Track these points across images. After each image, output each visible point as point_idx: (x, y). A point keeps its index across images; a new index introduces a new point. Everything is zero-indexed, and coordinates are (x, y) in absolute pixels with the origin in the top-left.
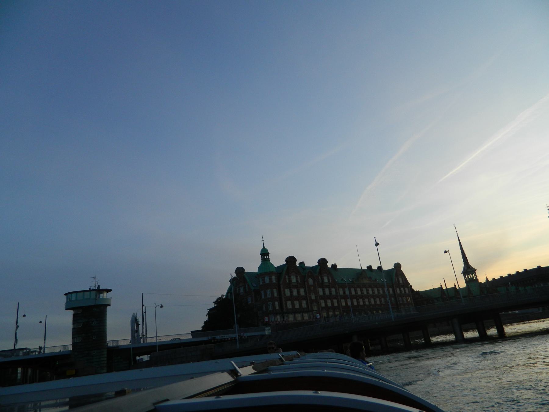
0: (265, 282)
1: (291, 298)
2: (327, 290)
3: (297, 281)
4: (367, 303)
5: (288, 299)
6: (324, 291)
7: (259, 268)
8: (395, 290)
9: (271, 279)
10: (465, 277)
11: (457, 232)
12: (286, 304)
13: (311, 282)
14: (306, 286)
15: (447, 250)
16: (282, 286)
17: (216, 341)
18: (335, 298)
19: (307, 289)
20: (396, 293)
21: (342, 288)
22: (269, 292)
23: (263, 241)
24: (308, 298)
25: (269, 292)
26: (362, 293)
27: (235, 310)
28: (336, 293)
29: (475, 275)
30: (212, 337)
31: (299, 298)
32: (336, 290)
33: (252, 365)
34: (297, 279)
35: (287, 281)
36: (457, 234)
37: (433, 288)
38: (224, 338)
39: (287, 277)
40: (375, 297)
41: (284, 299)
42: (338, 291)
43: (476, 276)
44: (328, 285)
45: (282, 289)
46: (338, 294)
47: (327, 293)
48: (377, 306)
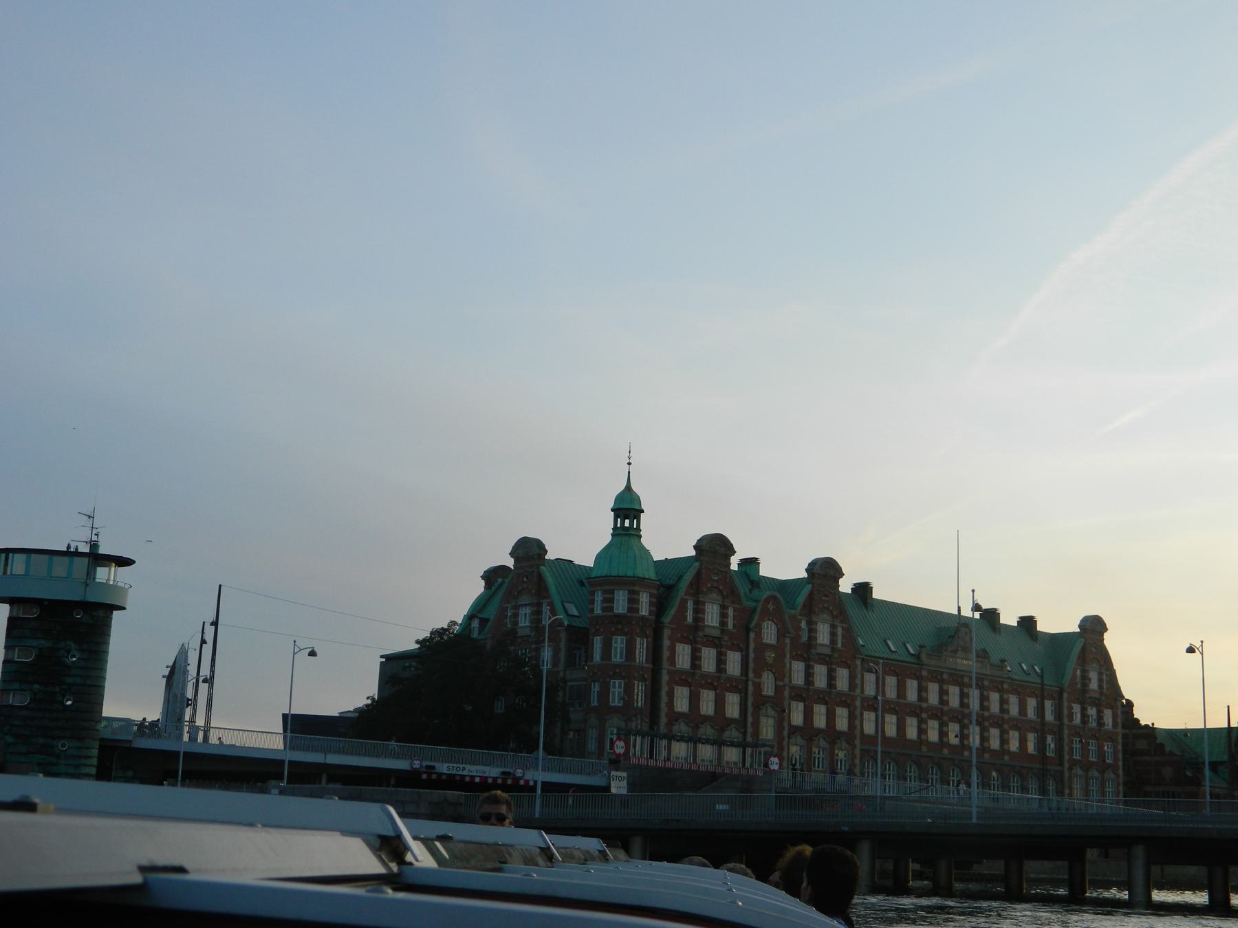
0: (612, 609)
1: (693, 679)
2: (820, 671)
3: (723, 624)
9: (633, 601)
13: (769, 633)
14: (752, 645)
15: (1198, 644)
16: (667, 633)
18: (734, 689)
19: (752, 655)
20: (1066, 721)
22: (619, 643)
23: (629, 464)
24: (751, 688)
25: (619, 643)
26: (1003, 710)
28: (852, 686)
30: (425, 764)
31: (720, 683)
34: (723, 615)
35: (690, 619)
38: (460, 773)
39: (690, 605)
40: (945, 718)
41: (665, 678)
42: (858, 681)
44: (1098, 699)
45: (666, 643)
46: (858, 691)
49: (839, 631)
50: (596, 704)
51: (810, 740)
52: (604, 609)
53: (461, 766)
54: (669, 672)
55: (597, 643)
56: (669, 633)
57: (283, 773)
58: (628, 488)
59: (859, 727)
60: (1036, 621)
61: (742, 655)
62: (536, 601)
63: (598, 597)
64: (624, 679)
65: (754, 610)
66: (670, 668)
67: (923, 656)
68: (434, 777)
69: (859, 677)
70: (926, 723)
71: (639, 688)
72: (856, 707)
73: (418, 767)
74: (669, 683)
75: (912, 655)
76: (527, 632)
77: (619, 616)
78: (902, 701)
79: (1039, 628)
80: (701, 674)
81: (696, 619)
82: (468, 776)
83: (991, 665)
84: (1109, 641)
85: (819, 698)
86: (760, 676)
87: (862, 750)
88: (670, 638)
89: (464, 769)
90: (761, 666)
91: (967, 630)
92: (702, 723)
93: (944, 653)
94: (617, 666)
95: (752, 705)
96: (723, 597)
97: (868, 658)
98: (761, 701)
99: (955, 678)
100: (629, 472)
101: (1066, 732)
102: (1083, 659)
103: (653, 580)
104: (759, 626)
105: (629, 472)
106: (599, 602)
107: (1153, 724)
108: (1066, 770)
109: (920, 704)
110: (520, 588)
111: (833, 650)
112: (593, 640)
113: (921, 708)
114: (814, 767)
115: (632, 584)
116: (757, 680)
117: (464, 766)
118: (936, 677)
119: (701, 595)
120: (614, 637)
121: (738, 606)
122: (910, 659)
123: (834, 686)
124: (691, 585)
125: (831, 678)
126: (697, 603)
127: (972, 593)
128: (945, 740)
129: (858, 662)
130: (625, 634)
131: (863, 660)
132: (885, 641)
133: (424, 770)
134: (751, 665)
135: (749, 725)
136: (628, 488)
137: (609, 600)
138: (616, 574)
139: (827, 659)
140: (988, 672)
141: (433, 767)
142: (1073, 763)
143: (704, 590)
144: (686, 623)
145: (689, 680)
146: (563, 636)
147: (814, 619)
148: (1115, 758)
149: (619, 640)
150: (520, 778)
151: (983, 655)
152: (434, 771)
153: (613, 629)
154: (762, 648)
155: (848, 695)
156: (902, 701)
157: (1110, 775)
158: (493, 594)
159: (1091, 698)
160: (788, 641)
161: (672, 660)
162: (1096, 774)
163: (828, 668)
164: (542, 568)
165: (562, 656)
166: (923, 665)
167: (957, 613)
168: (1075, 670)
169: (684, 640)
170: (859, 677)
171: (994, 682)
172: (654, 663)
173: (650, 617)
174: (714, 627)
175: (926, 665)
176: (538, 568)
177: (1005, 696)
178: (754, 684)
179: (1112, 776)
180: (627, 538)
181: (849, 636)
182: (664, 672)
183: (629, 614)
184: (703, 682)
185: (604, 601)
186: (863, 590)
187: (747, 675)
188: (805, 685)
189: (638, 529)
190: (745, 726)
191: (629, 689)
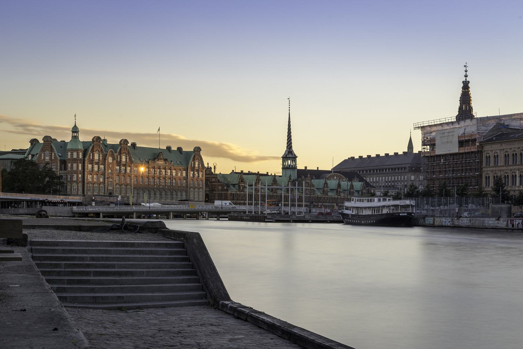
8: (189, 174)
9: (78, 155)
11: (289, 108)
14: (106, 163)
16: (86, 162)
17: (62, 202)
20: (189, 176)
22: (75, 165)
23: (75, 119)
24: (106, 174)
33: (496, 218)
35: (91, 158)
36: (289, 110)
37: (220, 173)
39: (91, 154)
41: (86, 173)
45: (86, 164)
46: (133, 172)
48: (166, 187)
52: (71, 157)
54: (87, 172)
58: (75, 125)
62: (50, 153)
65: (107, 154)
75: (147, 162)
76: (48, 160)
87: (133, 188)
88: (87, 163)
89: (53, 199)
91: (162, 154)
97: (114, 315)
124: (91, 149)
127: (295, 149)
130: (76, 163)
132: (140, 159)
134: (106, 168)
135: (106, 183)
136: (75, 125)
137: (72, 155)
142: (191, 187)
146: (59, 162)
147: (121, 155)
148: (203, 185)
150: (64, 201)
154: (109, 164)
157: (201, 190)
158: (33, 147)
159: (196, 169)
160: (115, 161)
162: (192, 190)
164: (52, 144)
165: (59, 167)
168: (192, 162)
176: (51, 144)
179: (202, 190)
180: (76, 139)
182: (86, 172)
185: (71, 155)
186: (134, 145)
187: (105, 171)
191: (77, 176)
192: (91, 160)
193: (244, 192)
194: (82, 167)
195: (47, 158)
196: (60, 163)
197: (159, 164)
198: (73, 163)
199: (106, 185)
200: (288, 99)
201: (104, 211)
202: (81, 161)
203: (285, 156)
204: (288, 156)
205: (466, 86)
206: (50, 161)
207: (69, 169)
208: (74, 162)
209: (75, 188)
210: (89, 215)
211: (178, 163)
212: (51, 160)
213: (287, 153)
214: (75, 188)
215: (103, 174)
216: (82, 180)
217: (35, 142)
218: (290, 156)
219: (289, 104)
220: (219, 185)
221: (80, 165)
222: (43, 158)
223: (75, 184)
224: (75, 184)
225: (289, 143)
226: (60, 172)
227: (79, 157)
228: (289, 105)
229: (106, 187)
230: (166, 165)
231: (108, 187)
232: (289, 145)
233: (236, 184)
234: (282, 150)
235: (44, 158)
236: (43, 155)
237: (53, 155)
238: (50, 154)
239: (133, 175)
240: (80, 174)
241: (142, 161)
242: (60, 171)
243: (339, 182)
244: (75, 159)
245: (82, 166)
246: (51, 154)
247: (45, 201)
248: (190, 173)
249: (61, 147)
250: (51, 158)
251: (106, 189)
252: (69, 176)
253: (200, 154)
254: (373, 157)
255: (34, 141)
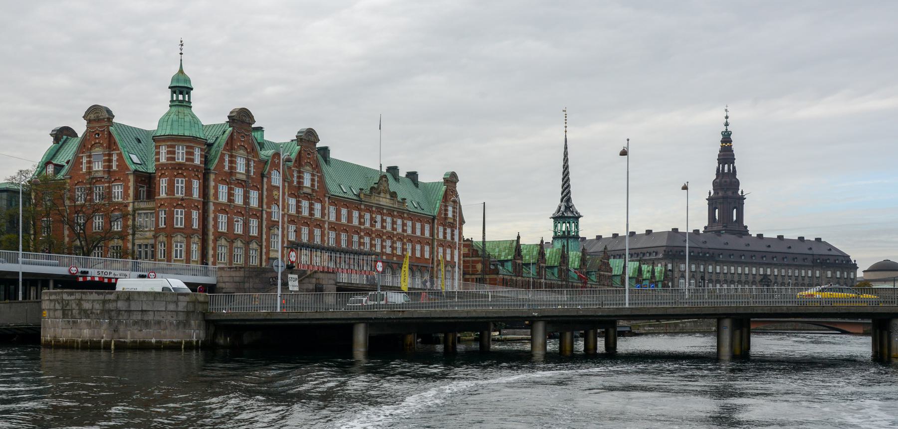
0: (174, 159)
1: (227, 209)
2: (239, 193)
3: (248, 171)
4: (388, 250)
5: (222, 209)
6: (230, 195)
7: (162, 122)
8: (436, 231)
10: (556, 226)
11: (566, 127)
12: (216, 219)
13: (277, 179)
14: (265, 187)
16: (212, 177)
18: (428, 244)
19: (265, 193)
20: (436, 237)
21: (421, 222)
22: (180, 183)
23: (181, 54)
24: (265, 216)
25: (180, 183)
27: (21, 199)
28: (323, 215)
29: (577, 226)
30: (80, 269)
31: (246, 212)
32: (323, 208)
34: (248, 165)
36: (566, 132)
38: (108, 276)
39: (227, 158)
40: (374, 235)
41: (212, 208)
42: (326, 211)
43: (578, 229)
45: (212, 184)
46: (326, 218)
47: (239, 200)
49: (316, 179)
50: (163, 226)
51: (232, 242)
52: (168, 159)
53: (108, 271)
55: (163, 183)
56: (214, 177)
57: (18, 280)
58: (181, 71)
59: (327, 242)
60: (329, 150)
61: (259, 193)
63: (162, 150)
64: (184, 209)
66: (214, 201)
67: (362, 196)
68: (89, 279)
69: (327, 208)
70: (363, 239)
71: (195, 215)
72: (325, 228)
73: (75, 272)
74: (214, 212)
76: (100, 175)
77: (180, 164)
78: (349, 224)
79: (331, 156)
80: (234, 206)
81: (231, 168)
82: (113, 278)
83: (398, 202)
84: (459, 187)
85: (178, 204)
86: (270, 208)
88: (214, 180)
89: (110, 273)
90: (273, 201)
92: (236, 239)
93: (374, 194)
94: (178, 199)
95: (266, 227)
96: (248, 153)
98: (273, 225)
99: (368, 208)
100: (181, 60)
101: (436, 243)
102: (446, 198)
103: (202, 139)
104: (269, 173)
105: (181, 60)
106: (164, 154)
107: (472, 239)
108: (435, 267)
109: (360, 226)
110: (93, 143)
111: (313, 190)
112: (160, 180)
113: (361, 229)
114: (234, 261)
115: (190, 141)
116: (268, 210)
117: (110, 271)
118: (369, 209)
119: (233, 151)
120: (176, 179)
121: (256, 159)
122: (355, 198)
123: (233, 201)
125: (246, 197)
126: (231, 156)
127: (577, 203)
128: (374, 249)
129: (327, 199)
131: (329, 198)
133: (79, 274)
134: (265, 200)
135: (264, 240)
136: (181, 71)
138: (176, 134)
139: (309, 197)
140: (396, 206)
141: (87, 272)
142: (219, 236)
143: (236, 147)
144: (224, 170)
145: (227, 210)
146: (131, 178)
149: (180, 181)
151: (393, 195)
152: (88, 275)
153: (175, 174)
154: (272, 188)
155: (411, 236)
156: (349, 224)
158: (61, 147)
161: (216, 195)
163: (309, 203)
164: (111, 128)
165: (131, 192)
166: (362, 201)
167: (379, 169)
169: (224, 182)
170: (327, 208)
171: (400, 212)
172: (204, 198)
173: (201, 165)
174: (308, 188)
175: (364, 201)
177: (405, 222)
178: (267, 212)
181: (322, 181)
182: (211, 204)
183: (187, 163)
184: (193, 206)
185: (169, 152)
187: (262, 207)
188: (296, 214)
189: (189, 102)
190: (261, 241)
192: (225, 172)
193: (522, 277)
194: (202, 190)
195: (98, 167)
196: (136, 181)
197: (381, 203)
198: (175, 176)
199: (264, 247)
200: (564, 111)
201: (329, 317)
202: (197, 171)
203: (560, 215)
204: (566, 215)
205: (727, 138)
206: (106, 176)
207: (163, 195)
208: (178, 174)
209: (179, 249)
210: (497, 337)
211: (415, 206)
212: (109, 172)
213: (563, 209)
214: (181, 251)
215: (256, 215)
216: (201, 227)
217: (67, 135)
218: (570, 214)
219: (566, 120)
220: (477, 262)
221: (196, 184)
222: (84, 170)
223: (179, 236)
224: (179, 236)
225: (567, 191)
226: (137, 207)
227: (193, 160)
228: (566, 123)
229: (264, 250)
230: (395, 206)
231: (268, 253)
232: (565, 196)
233: (507, 261)
234: (554, 203)
235: (90, 168)
236: (85, 160)
237: (115, 158)
238: (105, 155)
239: (327, 223)
240: (196, 208)
241: (345, 191)
242: (136, 203)
243: (640, 265)
244: (180, 166)
245: (202, 186)
246: (110, 155)
247: (77, 277)
248: (216, 188)
249: (139, 141)
250: (110, 167)
251: (264, 257)
252: (163, 216)
253: (455, 188)
254: (592, 241)
255: (65, 132)
